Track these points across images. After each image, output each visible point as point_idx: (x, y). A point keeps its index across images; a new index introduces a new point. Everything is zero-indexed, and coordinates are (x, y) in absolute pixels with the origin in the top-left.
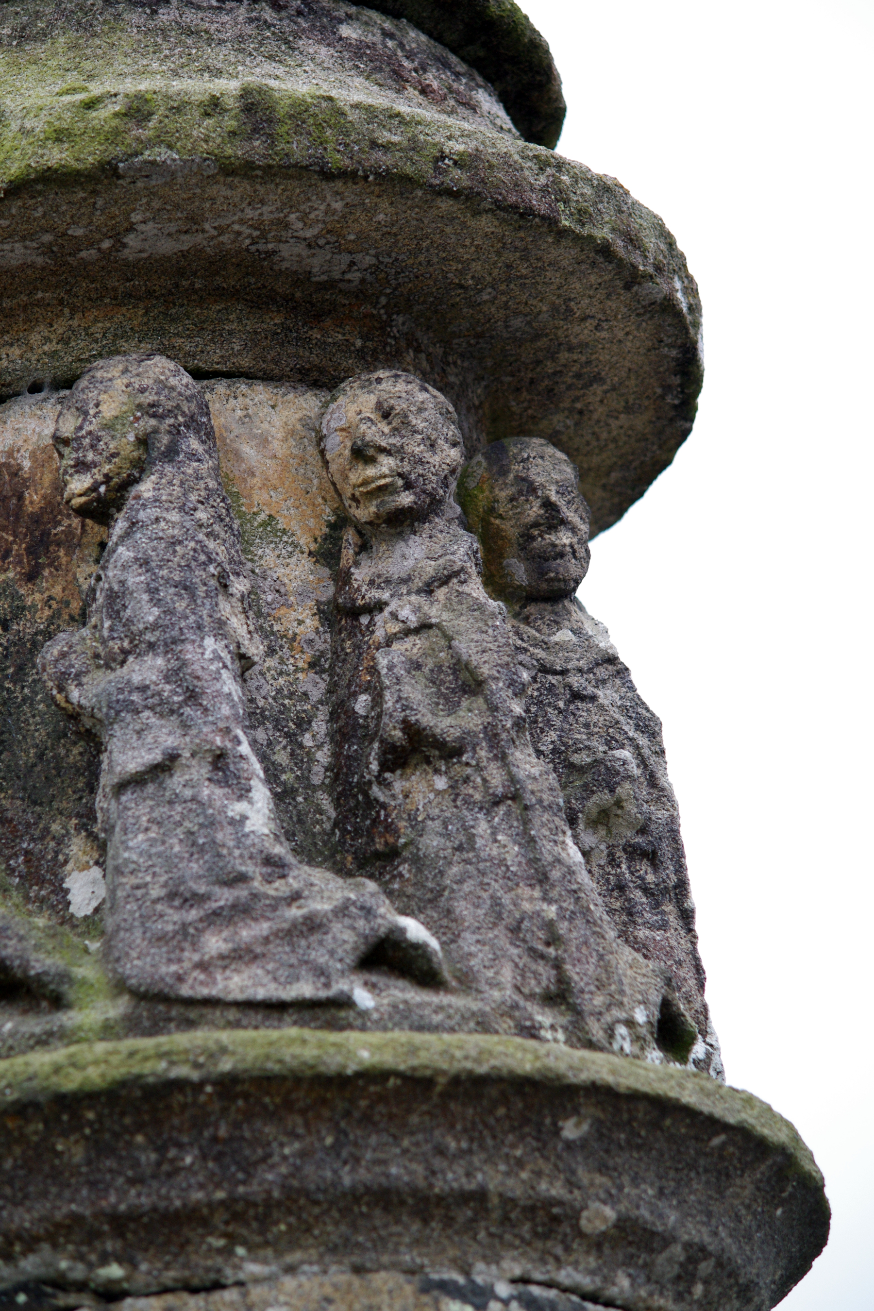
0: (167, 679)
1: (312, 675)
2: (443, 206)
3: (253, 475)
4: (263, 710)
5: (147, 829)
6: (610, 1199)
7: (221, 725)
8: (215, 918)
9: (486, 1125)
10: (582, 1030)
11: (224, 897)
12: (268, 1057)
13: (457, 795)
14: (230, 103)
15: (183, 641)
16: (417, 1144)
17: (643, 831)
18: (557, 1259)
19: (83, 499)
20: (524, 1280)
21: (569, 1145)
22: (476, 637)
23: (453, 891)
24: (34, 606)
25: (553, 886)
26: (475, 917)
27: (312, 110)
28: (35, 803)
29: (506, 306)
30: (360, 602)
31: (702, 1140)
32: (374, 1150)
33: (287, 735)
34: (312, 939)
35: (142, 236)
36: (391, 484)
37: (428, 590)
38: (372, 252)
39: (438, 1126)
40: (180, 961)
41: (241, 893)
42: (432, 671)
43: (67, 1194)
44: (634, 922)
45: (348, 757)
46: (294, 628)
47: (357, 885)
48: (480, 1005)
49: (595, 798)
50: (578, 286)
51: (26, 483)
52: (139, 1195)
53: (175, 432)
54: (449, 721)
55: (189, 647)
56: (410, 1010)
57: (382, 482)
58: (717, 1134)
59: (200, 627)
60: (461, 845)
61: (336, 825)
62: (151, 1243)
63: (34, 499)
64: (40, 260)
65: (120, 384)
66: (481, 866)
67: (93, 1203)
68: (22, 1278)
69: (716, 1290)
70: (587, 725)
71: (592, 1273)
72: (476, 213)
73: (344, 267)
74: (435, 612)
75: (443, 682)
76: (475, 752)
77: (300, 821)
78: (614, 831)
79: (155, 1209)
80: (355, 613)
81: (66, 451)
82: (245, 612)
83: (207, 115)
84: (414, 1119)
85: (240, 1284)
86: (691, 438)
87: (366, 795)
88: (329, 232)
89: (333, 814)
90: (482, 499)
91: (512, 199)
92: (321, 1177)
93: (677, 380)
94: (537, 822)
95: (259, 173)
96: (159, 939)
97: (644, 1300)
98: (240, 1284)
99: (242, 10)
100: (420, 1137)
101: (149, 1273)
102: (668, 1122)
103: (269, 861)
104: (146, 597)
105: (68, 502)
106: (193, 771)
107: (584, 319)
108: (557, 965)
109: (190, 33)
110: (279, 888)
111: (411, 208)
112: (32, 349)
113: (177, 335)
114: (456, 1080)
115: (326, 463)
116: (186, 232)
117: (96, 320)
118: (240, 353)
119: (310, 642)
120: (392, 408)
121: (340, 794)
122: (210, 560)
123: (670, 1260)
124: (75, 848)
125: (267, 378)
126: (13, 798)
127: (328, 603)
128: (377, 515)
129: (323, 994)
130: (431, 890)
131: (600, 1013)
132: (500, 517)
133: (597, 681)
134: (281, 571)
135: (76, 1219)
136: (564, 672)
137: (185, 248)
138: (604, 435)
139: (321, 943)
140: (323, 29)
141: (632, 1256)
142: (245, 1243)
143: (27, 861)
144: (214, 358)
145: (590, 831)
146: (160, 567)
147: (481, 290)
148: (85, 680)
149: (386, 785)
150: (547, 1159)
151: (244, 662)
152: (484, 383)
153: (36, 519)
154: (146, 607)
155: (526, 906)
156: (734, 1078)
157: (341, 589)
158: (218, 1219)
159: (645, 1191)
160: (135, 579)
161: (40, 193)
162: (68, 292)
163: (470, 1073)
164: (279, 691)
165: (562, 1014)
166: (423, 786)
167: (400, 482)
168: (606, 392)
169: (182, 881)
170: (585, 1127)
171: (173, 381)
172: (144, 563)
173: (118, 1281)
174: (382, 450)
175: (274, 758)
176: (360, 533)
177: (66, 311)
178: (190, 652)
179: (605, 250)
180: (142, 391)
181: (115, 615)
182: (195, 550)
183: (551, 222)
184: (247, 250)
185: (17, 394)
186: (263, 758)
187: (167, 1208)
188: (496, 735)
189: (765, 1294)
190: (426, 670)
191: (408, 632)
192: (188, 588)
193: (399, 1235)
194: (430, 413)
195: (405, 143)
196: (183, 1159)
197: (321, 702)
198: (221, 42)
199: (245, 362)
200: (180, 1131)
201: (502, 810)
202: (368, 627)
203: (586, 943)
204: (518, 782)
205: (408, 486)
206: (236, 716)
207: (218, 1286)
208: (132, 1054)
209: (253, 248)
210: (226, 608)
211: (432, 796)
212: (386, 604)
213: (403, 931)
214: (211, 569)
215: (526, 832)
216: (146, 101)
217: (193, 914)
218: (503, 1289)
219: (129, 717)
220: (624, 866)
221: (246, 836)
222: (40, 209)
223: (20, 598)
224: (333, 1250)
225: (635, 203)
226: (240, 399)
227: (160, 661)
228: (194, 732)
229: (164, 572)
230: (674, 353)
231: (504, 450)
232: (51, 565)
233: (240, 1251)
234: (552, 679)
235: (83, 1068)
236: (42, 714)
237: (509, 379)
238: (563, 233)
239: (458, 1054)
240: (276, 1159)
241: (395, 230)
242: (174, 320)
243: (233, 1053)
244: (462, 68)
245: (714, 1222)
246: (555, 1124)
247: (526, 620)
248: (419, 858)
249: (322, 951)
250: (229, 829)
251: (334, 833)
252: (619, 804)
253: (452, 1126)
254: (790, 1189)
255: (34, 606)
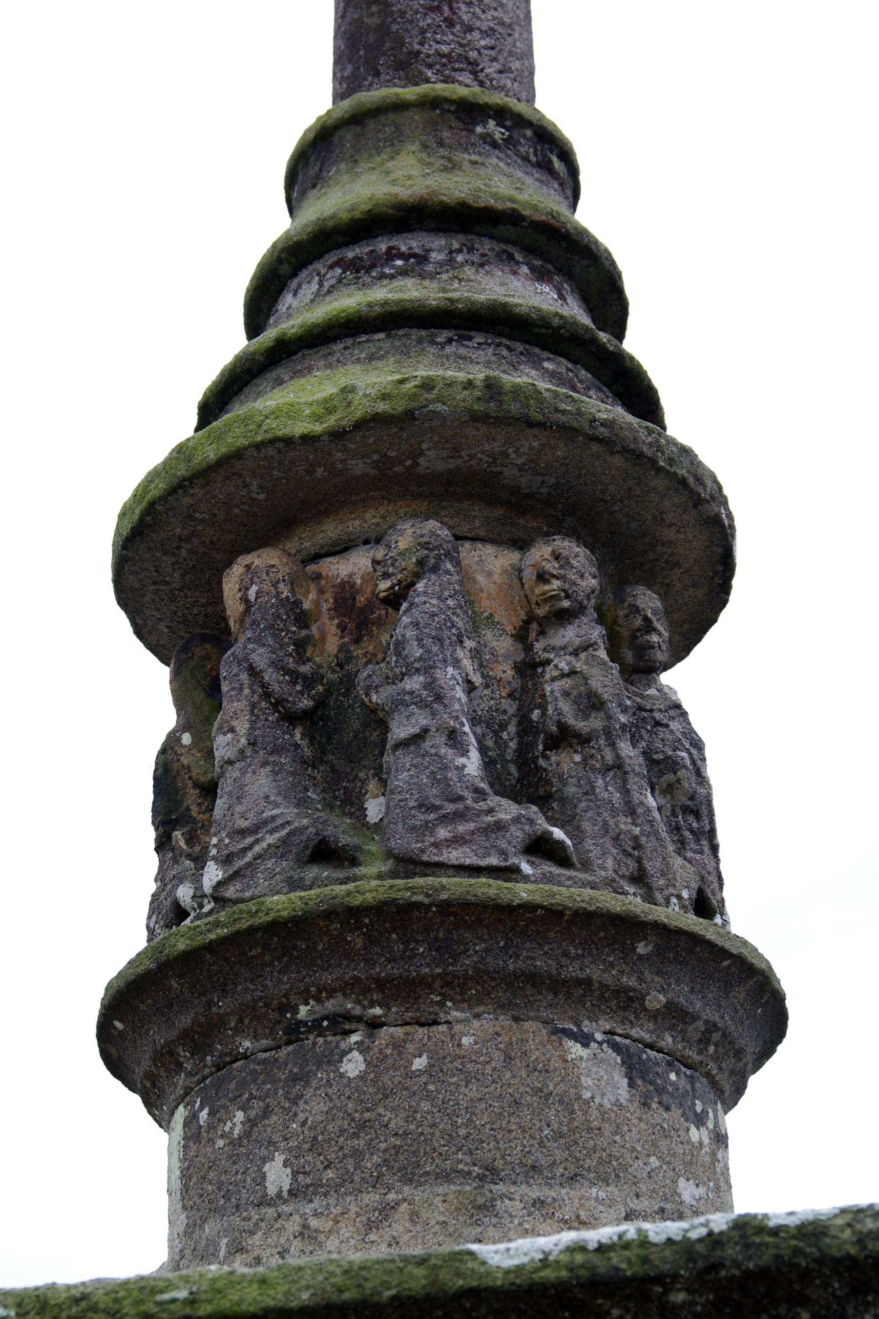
0: (425, 688)
1: (509, 701)
2: (594, 448)
3: (482, 591)
4: (481, 717)
5: (409, 770)
6: (662, 990)
7: (454, 714)
8: (444, 819)
9: (593, 942)
10: (651, 897)
11: (450, 808)
12: (468, 893)
13: (587, 765)
14: (479, 383)
15: (435, 667)
16: (552, 949)
17: (692, 798)
18: (631, 1022)
19: (386, 593)
20: (612, 1033)
21: (640, 957)
22: (601, 679)
23: (581, 816)
24: (358, 656)
25: (638, 817)
26: (593, 831)
27: (523, 389)
28: (351, 761)
29: (628, 515)
30: (538, 660)
31: (718, 962)
32: (528, 951)
33: (493, 731)
34: (498, 834)
35: (428, 459)
36: (558, 595)
37: (576, 653)
38: (554, 475)
39: (565, 940)
40: (423, 841)
41: (460, 806)
42: (576, 697)
43: (352, 965)
44: (685, 848)
45: (527, 744)
46: (500, 674)
47: (527, 808)
48: (593, 878)
49: (665, 777)
50: (668, 504)
51: (358, 592)
52: (393, 968)
53: (438, 558)
54: (583, 724)
55: (438, 671)
56: (553, 878)
57: (553, 593)
58: (726, 959)
59: (445, 661)
60: (587, 791)
61: (518, 781)
62: (399, 996)
63: (361, 600)
64: (372, 472)
65: (409, 532)
66: (598, 803)
67: (366, 971)
68: (326, 1012)
69: (721, 1051)
70: (663, 740)
71: (651, 1032)
72: (612, 453)
73: (538, 484)
74: (579, 666)
75: (581, 703)
76: (597, 741)
77: (498, 778)
78: (676, 797)
79: (401, 977)
80: (534, 665)
81: (378, 568)
82: (471, 658)
83: (465, 388)
84: (551, 935)
85: (448, 1022)
86: (728, 606)
87: (536, 764)
88: (531, 461)
89: (516, 775)
90: (610, 616)
91: (633, 446)
92: (496, 964)
93: (720, 568)
94: (631, 781)
95: (492, 420)
96: (412, 829)
97: (680, 1051)
98: (448, 1022)
99: (491, 350)
100: (555, 945)
101: (397, 1013)
102: (698, 949)
103: (477, 790)
104: (416, 643)
105: (378, 595)
106: (437, 739)
107: (670, 525)
108: (639, 860)
109: (461, 358)
110: (483, 805)
111: (576, 448)
112: (366, 521)
113: (445, 516)
114: (576, 913)
115: (523, 585)
116: (452, 457)
117: (401, 507)
118: (479, 528)
119: (509, 683)
120: (560, 554)
121: (521, 764)
122: (453, 626)
123: (696, 1029)
124: (371, 786)
125: (493, 542)
126: (339, 759)
127: (521, 662)
128: (549, 612)
129: (503, 864)
130: (569, 816)
131: (662, 889)
132: (620, 626)
133: (670, 717)
134: (495, 644)
135: (357, 979)
136: (651, 711)
137: (451, 467)
138: (680, 601)
139: (504, 836)
140: (534, 362)
141: (674, 1025)
142: (451, 1000)
143: (345, 793)
144: (465, 529)
145: (662, 796)
146: (425, 628)
147: (614, 504)
148: (380, 690)
149: (547, 758)
150: (628, 964)
151: (470, 687)
152: (615, 563)
153: (362, 610)
154: (416, 649)
155: (623, 826)
156: (735, 928)
157: (528, 653)
158: (438, 984)
159: (683, 989)
160: (410, 633)
161: (372, 428)
162: (387, 492)
163: (585, 909)
164: (490, 708)
165: (640, 888)
166: (567, 759)
167: (563, 594)
168: (682, 573)
169: (427, 798)
170: (650, 948)
171: (439, 532)
172: (416, 625)
173: (380, 1017)
174: (554, 576)
175: (485, 743)
176: (540, 625)
177: (386, 502)
178: (439, 674)
179: (683, 482)
180: (422, 536)
181: (398, 654)
182: (445, 620)
183: (653, 462)
184: (486, 470)
185: (357, 545)
186: (479, 742)
187: (408, 976)
188: (610, 732)
189: (749, 1058)
190: (572, 696)
191: (563, 676)
192: (439, 640)
193: (540, 1001)
194: (582, 558)
195: (574, 411)
196: (418, 950)
197: (513, 715)
198: (478, 363)
199: (482, 533)
200: (417, 933)
201: (611, 774)
202: (541, 674)
203: (656, 850)
204: (621, 758)
205: (567, 597)
206: (463, 711)
207: (436, 1023)
208: (391, 887)
209: (489, 469)
210: (460, 653)
211: (572, 765)
212: (552, 661)
213: (551, 833)
214: (454, 631)
215: (624, 786)
216: (433, 380)
217: (432, 816)
218: (599, 1036)
219: (403, 709)
220: (680, 817)
221: (465, 776)
222: (372, 438)
223: (351, 652)
224: (502, 1006)
225: (700, 462)
226: (478, 551)
227: (421, 678)
228: (438, 717)
229: (427, 630)
230: (720, 550)
231: (624, 590)
232: (368, 635)
233: (449, 1004)
234: (645, 714)
235: (364, 894)
236: (358, 714)
237: (628, 562)
238: (660, 469)
239: (578, 899)
240: (471, 952)
241: (567, 462)
242: (444, 508)
243: (449, 890)
244: (609, 394)
245: (722, 1010)
246: (632, 944)
247: (632, 683)
248: (563, 799)
249: (504, 841)
250: (455, 772)
251: (516, 786)
252: (678, 781)
253: (573, 941)
254: (766, 997)
255: (358, 656)
